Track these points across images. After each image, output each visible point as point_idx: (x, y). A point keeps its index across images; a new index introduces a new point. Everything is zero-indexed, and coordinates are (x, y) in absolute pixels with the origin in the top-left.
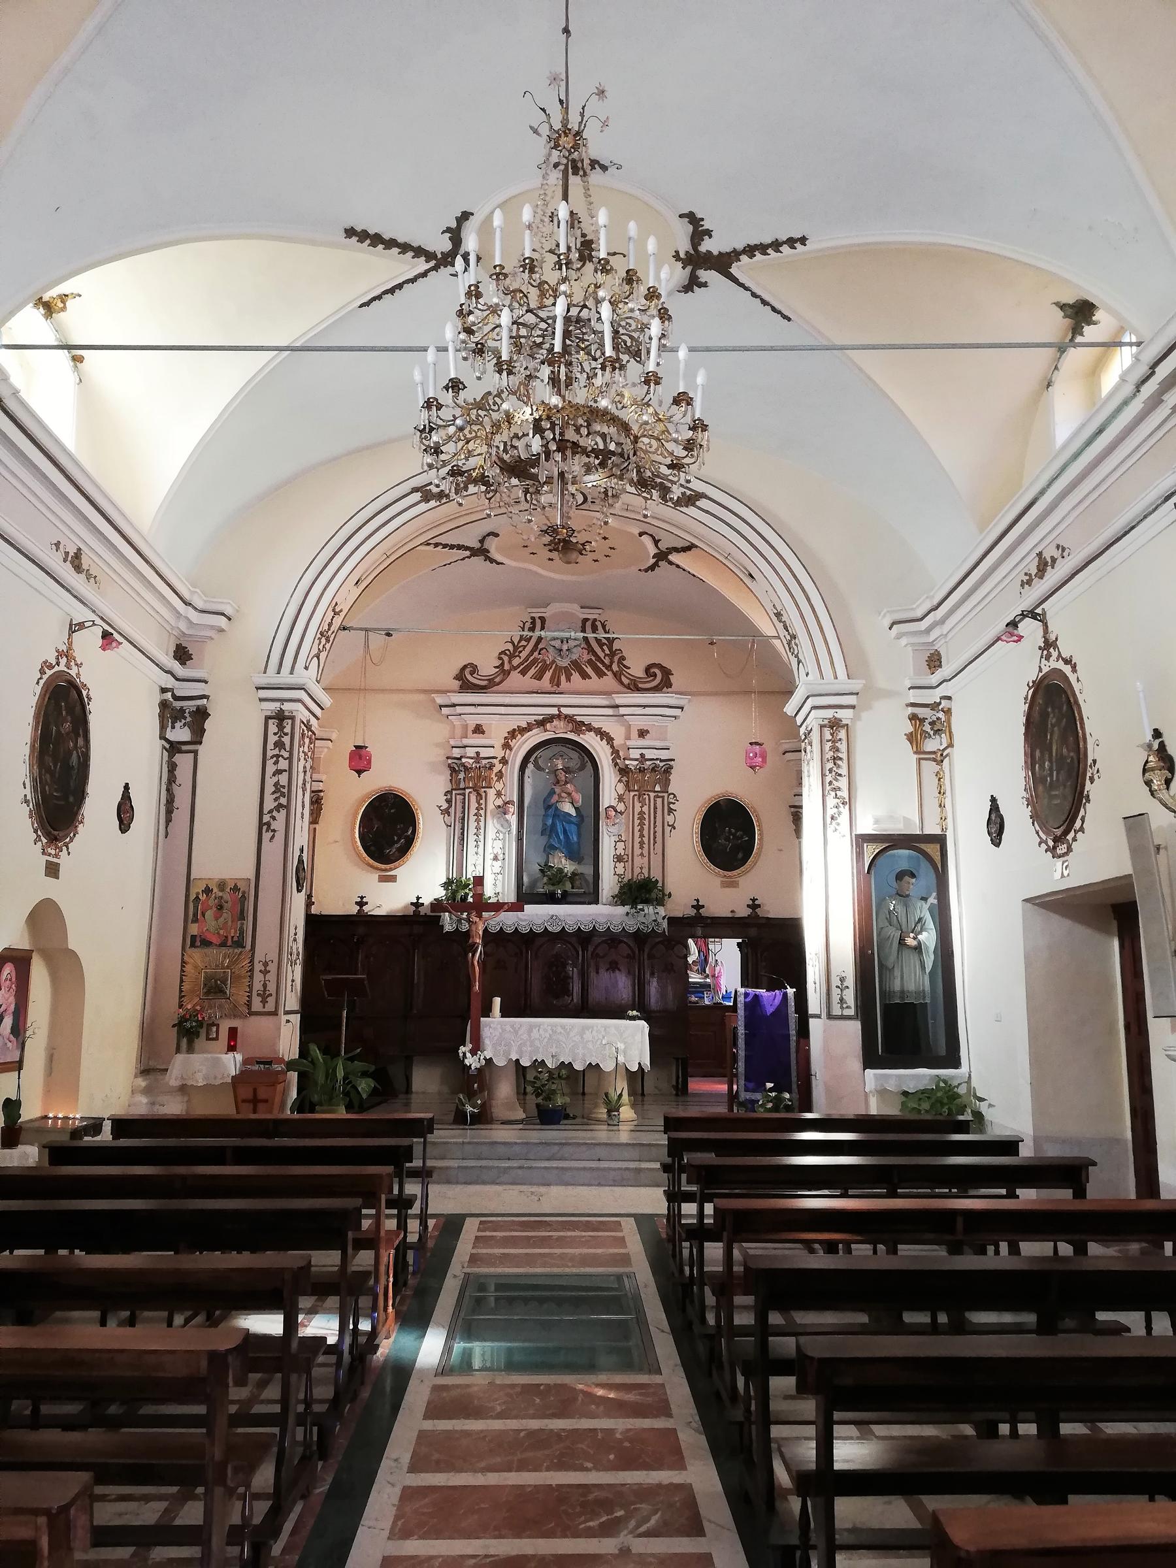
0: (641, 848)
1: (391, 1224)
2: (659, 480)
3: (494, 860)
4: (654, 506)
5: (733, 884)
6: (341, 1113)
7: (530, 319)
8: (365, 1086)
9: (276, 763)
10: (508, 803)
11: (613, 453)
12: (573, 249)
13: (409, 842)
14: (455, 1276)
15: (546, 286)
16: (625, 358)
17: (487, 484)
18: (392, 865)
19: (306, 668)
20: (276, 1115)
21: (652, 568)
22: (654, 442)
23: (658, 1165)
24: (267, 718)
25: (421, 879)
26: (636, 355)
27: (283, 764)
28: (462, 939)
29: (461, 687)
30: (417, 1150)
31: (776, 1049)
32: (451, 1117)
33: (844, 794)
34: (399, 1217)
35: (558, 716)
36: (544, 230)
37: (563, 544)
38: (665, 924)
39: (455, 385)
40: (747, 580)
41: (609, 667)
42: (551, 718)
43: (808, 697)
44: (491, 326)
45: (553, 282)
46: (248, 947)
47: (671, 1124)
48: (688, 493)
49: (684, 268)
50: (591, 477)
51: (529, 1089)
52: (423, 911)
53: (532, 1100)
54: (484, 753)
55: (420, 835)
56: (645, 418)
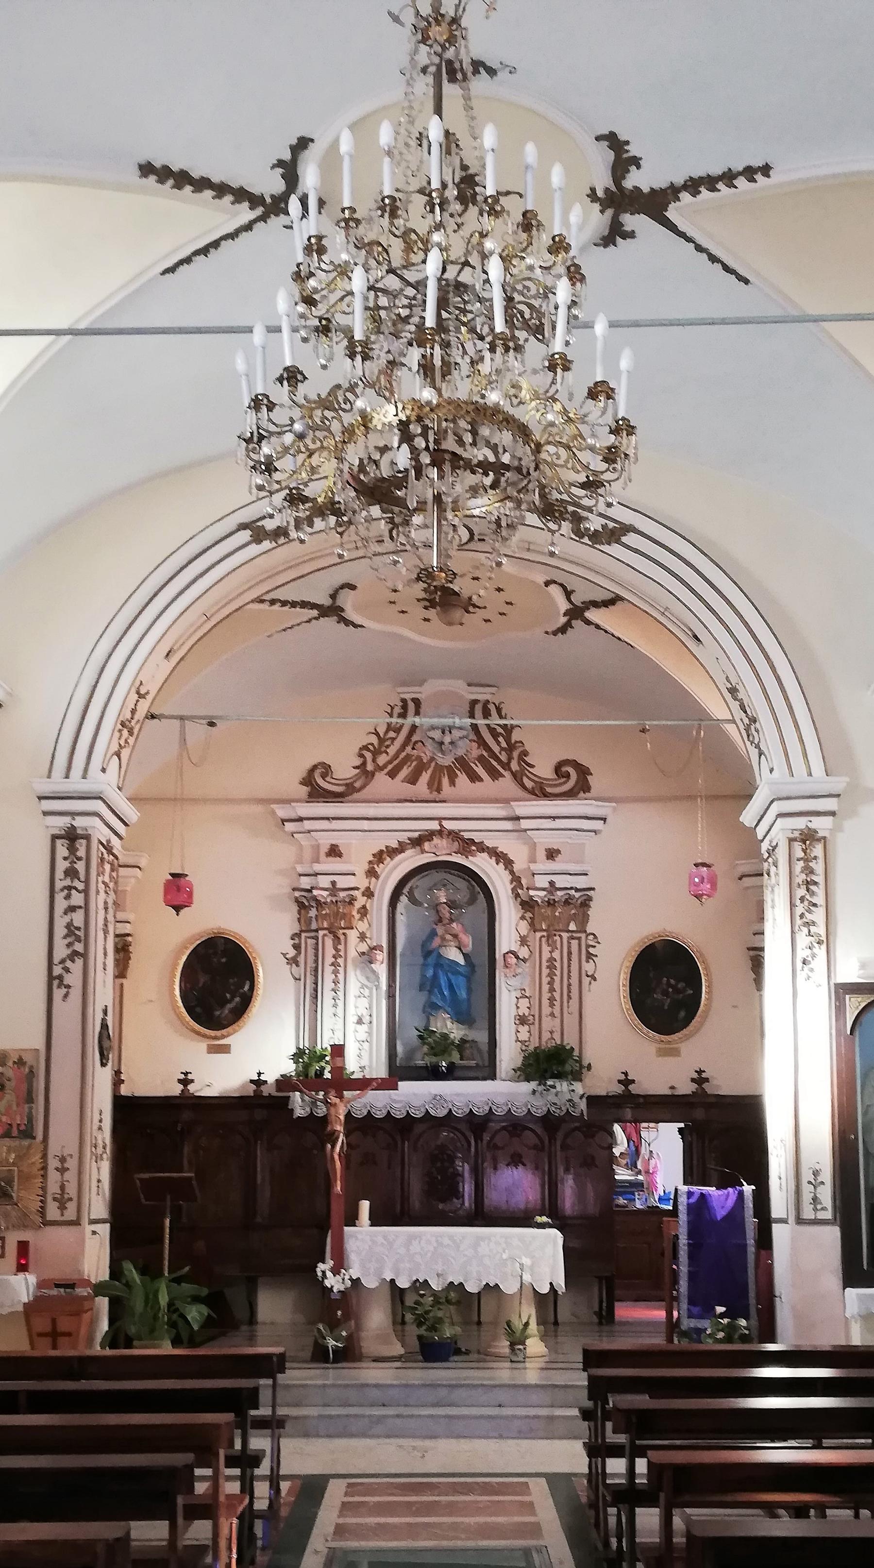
0: (552, 1005)
1: (233, 1488)
2: (571, 508)
3: (358, 1023)
4: (562, 540)
5: (674, 1052)
6: (166, 1349)
7: (392, 282)
8: (195, 1314)
9: (68, 897)
10: (375, 948)
11: (507, 467)
12: (450, 185)
13: (246, 1001)
14: (316, 1552)
15: (413, 236)
16: (521, 335)
17: (338, 513)
18: (224, 1032)
19: (104, 770)
20: (83, 1351)
21: (563, 630)
22: (562, 451)
23: (575, 1412)
24: (54, 838)
25: (260, 1051)
26: (538, 331)
27: (77, 899)
28: (317, 1126)
29: (310, 795)
30: (265, 1396)
31: (730, 1264)
32: (308, 1354)
33: (820, 929)
34: (242, 1478)
35: (440, 833)
36: (409, 157)
37: (442, 597)
38: (583, 1105)
39: (292, 376)
40: (691, 644)
41: (506, 766)
42: (429, 836)
43: (772, 802)
44: (339, 294)
45: (422, 230)
46: (40, 1136)
47: (591, 1359)
48: (611, 525)
49: (602, 212)
50: (479, 501)
51: (409, 1317)
52: (266, 1091)
53: (413, 1331)
54: (343, 882)
55: (260, 992)
56: (550, 417)
